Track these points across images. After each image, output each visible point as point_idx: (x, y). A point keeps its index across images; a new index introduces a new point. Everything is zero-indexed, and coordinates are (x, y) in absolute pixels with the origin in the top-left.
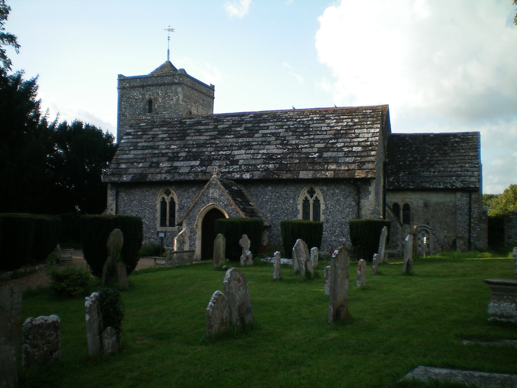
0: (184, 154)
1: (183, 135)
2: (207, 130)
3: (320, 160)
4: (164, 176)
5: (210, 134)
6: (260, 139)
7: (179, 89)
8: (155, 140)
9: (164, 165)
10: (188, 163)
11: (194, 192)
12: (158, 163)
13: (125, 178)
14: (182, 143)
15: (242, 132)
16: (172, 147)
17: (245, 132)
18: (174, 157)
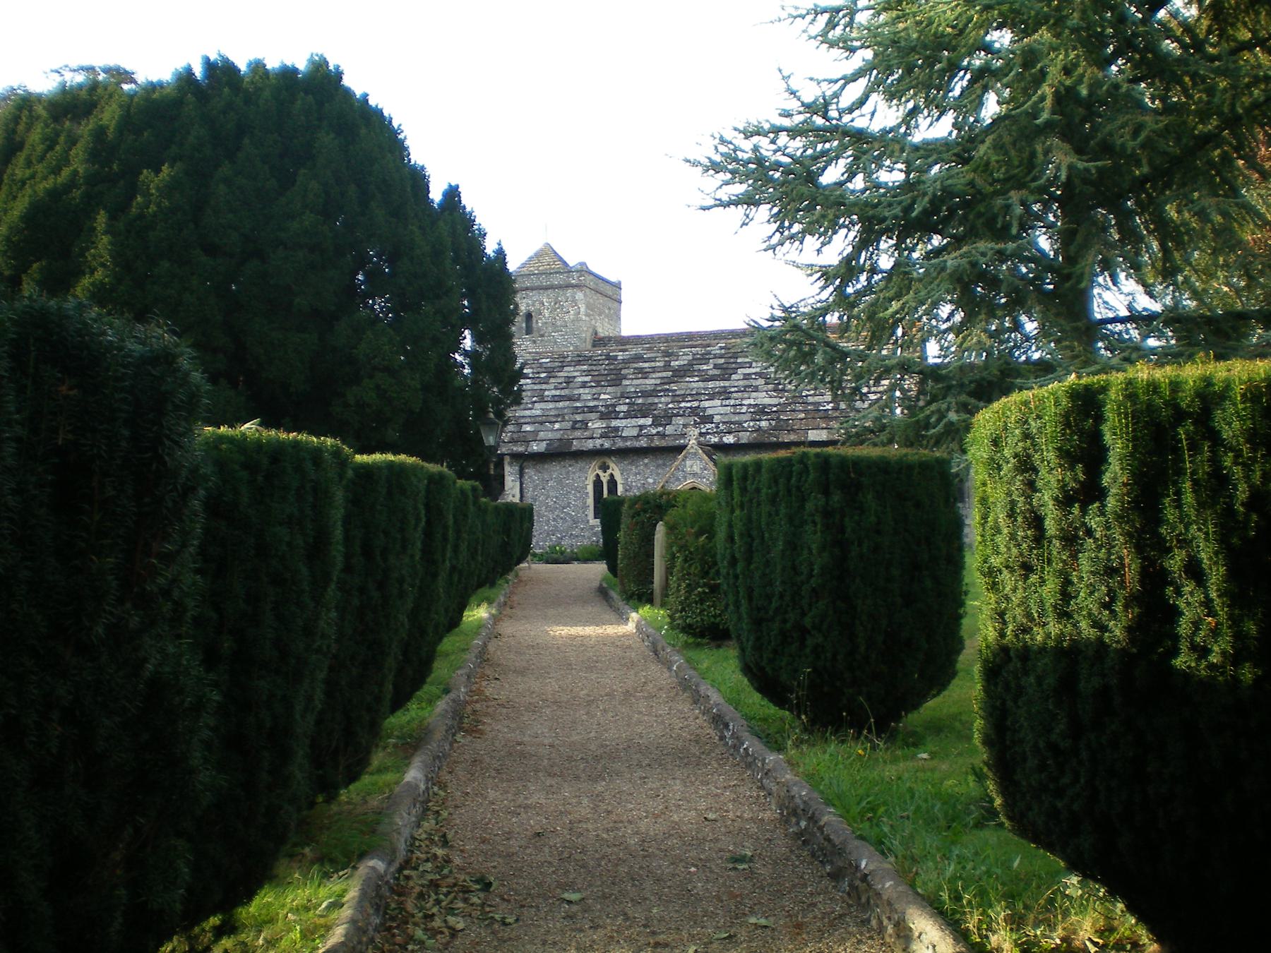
0: (624, 408)
1: (616, 379)
2: (654, 370)
3: (837, 414)
4: (598, 442)
5: (660, 375)
6: (741, 383)
7: (579, 295)
8: (571, 385)
9: (596, 426)
10: (634, 422)
11: (646, 465)
12: (585, 423)
13: (535, 447)
14: (618, 390)
15: (710, 373)
16: (603, 396)
17: (717, 372)
18: (609, 413)
